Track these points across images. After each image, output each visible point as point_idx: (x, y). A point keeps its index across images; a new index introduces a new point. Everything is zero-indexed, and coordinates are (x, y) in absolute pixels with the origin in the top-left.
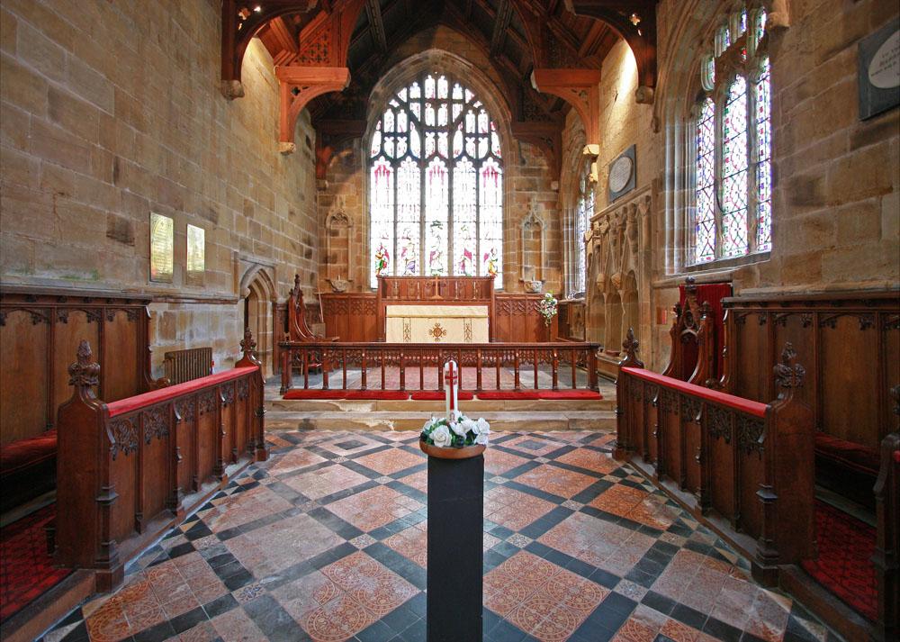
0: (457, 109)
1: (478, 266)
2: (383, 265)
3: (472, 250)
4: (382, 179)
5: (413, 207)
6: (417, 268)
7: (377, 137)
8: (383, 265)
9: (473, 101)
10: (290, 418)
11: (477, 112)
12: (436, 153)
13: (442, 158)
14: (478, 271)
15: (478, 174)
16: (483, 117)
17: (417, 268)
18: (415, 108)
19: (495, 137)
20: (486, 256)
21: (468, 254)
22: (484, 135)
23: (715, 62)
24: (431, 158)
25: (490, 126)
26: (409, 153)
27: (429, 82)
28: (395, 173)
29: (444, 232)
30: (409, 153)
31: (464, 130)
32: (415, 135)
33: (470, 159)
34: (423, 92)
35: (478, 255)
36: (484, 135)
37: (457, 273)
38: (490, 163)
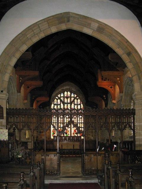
0: (73, 99)
7: (53, 105)
9: (76, 97)
11: (77, 99)
16: (79, 101)
18: (62, 98)
19: (82, 105)
25: (81, 102)
27: (66, 93)
31: (74, 103)
32: (62, 104)
34: (64, 95)
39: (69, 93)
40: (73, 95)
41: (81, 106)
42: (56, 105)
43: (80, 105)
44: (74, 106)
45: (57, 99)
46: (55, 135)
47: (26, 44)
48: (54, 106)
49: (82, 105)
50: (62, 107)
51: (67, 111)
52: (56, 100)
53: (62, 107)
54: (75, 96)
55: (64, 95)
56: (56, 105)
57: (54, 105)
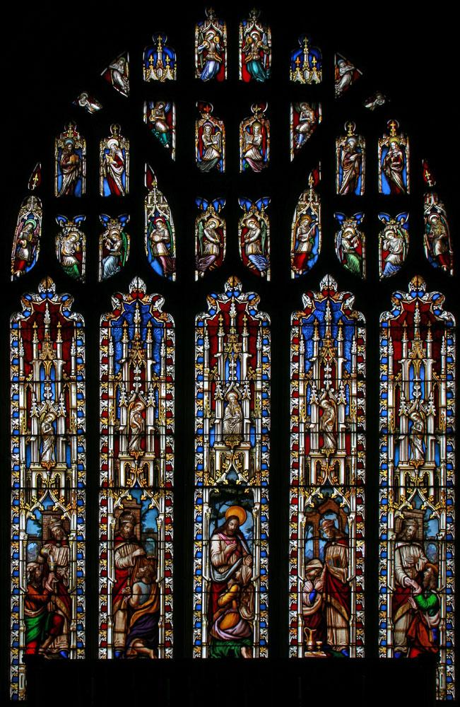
0: (305, 119)
1: (371, 627)
2: (51, 626)
3: (352, 573)
4: (50, 355)
5: (150, 442)
6: (165, 635)
7: (30, 218)
8: (51, 626)
9: (358, 90)
10: (24, 456)
11: (372, 131)
12: (233, 264)
13: (250, 280)
14: (372, 642)
15: (374, 330)
16: (393, 144)
17: (165, 635)
18: (158, 118)
19: (433, 207)
20: (401, 594)
21: (335, 590)
22: (396, 204)
23: (129, 291)
24: (214, 282)
25: (416, 175)
26: (137, 263)
27: (210, 35)
28: (92, 333)
29: (254, 521)
30: (137, 263)
31: (325, 191)
32: (156, 205)
33: (347, 280)
34: (185, 65)
35: (372, 591)
36: (396, 204)
37: (300, 646)
38: (416, 293)
39: (254, 34)
40: (306, 74)
41: (417, 229)
42: (349, 205)
43: (403, 218)
44: (330, 228)
45: (94, 131)
46: (61, 643)
47: (445, 541)
48: (50, 233)
49: (433, 207)
50: (160, 240)
51: (219, 355)
52: (71, 138)
53: (160, 240)
54: (344, 75)
55: (185, 65)
56: (349, 205)
57: (55, 208)
